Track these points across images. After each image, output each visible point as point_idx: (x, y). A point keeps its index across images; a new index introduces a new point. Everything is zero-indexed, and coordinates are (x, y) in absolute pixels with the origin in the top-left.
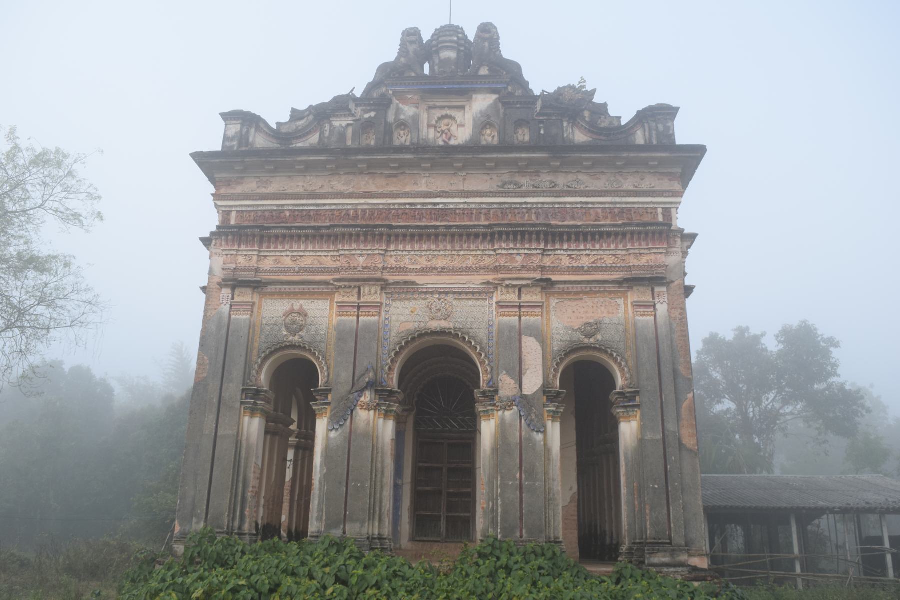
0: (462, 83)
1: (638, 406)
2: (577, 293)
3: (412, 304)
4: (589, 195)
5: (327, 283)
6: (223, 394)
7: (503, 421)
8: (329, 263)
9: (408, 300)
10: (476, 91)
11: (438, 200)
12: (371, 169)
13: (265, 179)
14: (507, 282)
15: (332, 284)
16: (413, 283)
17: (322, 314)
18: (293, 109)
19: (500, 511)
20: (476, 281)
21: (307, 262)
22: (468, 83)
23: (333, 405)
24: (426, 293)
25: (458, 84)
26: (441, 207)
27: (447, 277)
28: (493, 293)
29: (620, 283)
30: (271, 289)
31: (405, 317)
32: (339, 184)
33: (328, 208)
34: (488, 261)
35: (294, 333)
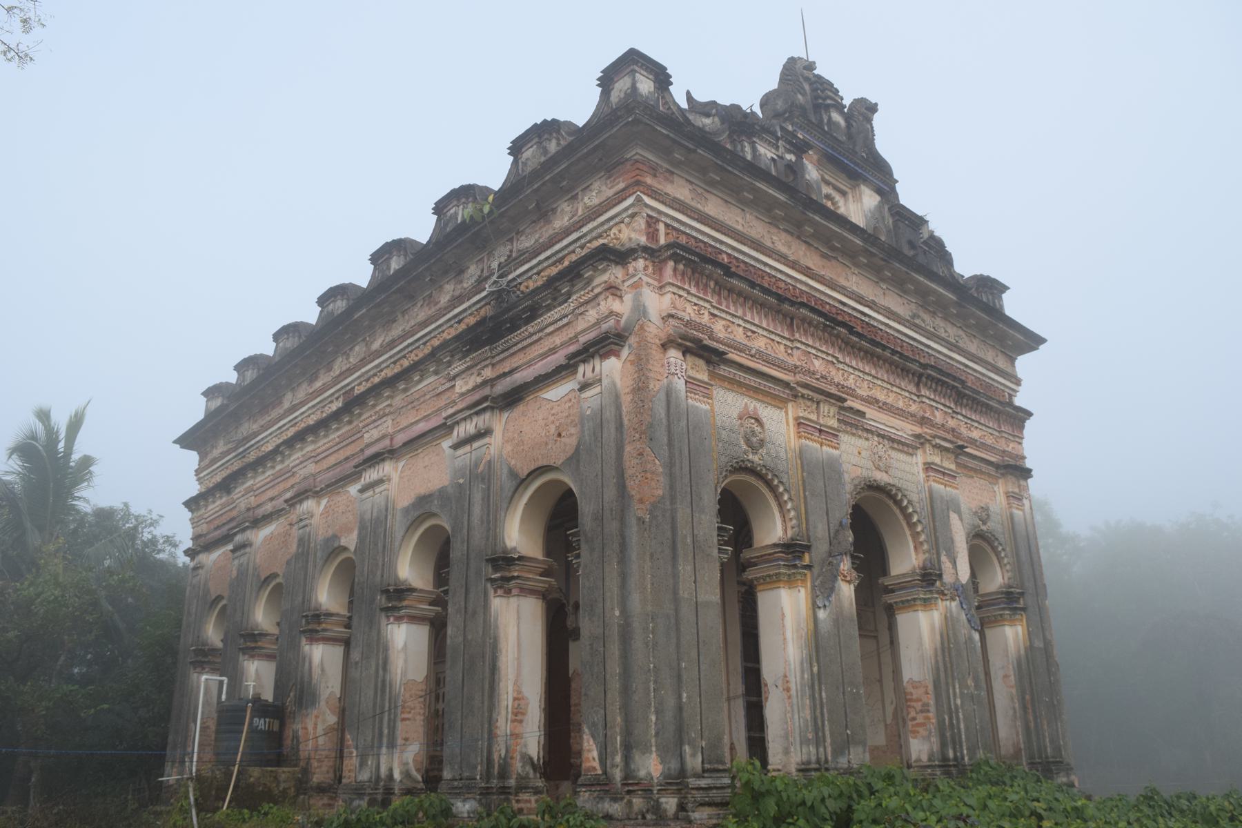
0: (857, 165)
1: (1023, 609)
2: (972, 469)
3: (862, 443)
4: (942, 342)
5: (787, 385)
6: (696, 532)
7: (948, 610)
8: (780, 352)
9: (853, 434)
10: (865, 181)
11: (866, 310)
12: (762, 206)
13: (700, 191)
14: (938, 441)
15: (792, 389)
16: (862, 414)
17: (780, 426)
18: (1029, 414)
19: (962, 726)
20: (905, 429)
21: (760, 344)
22: (862, 168)
23: (816, 570)
24: (867, 431)
25: (855, 163)
26: (867, 319)
27: (885, 417)
28: (917, 448)
29: (997, 466)
30: (724, 370)
31: (855, 457)
32: (780, 241)
33: (767, 270)
34: (914, 408)
35: (755, 450)
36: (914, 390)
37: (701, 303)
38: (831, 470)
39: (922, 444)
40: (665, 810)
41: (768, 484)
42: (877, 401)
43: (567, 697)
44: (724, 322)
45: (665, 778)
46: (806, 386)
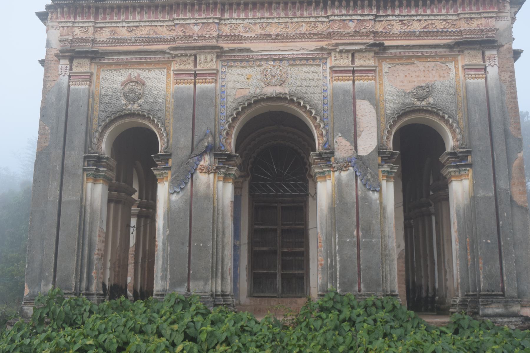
1: (470, 165)
5: (163, 52)
6: (65, 162)
7: (339, 181)
14: (341, 48)
15: (168, 53)
16: (248, 50)
17: (159, 83)
20: (309, 47)
21: (143, 32)
23: (173, 169)
24: (261, 60)
29: (450, 47)
30: (108, 59)
31: (241, 83)
34: (321, 28)
36: (323, 14)
37: (86, 24)
38: (213, 99)
39: (330, 54)
40: (27, 313)
41: (437, 115)
42: (269, 36)
43: (155, 238)
44: (110, 29)
45: (30, 297)
46: (176, 49)
